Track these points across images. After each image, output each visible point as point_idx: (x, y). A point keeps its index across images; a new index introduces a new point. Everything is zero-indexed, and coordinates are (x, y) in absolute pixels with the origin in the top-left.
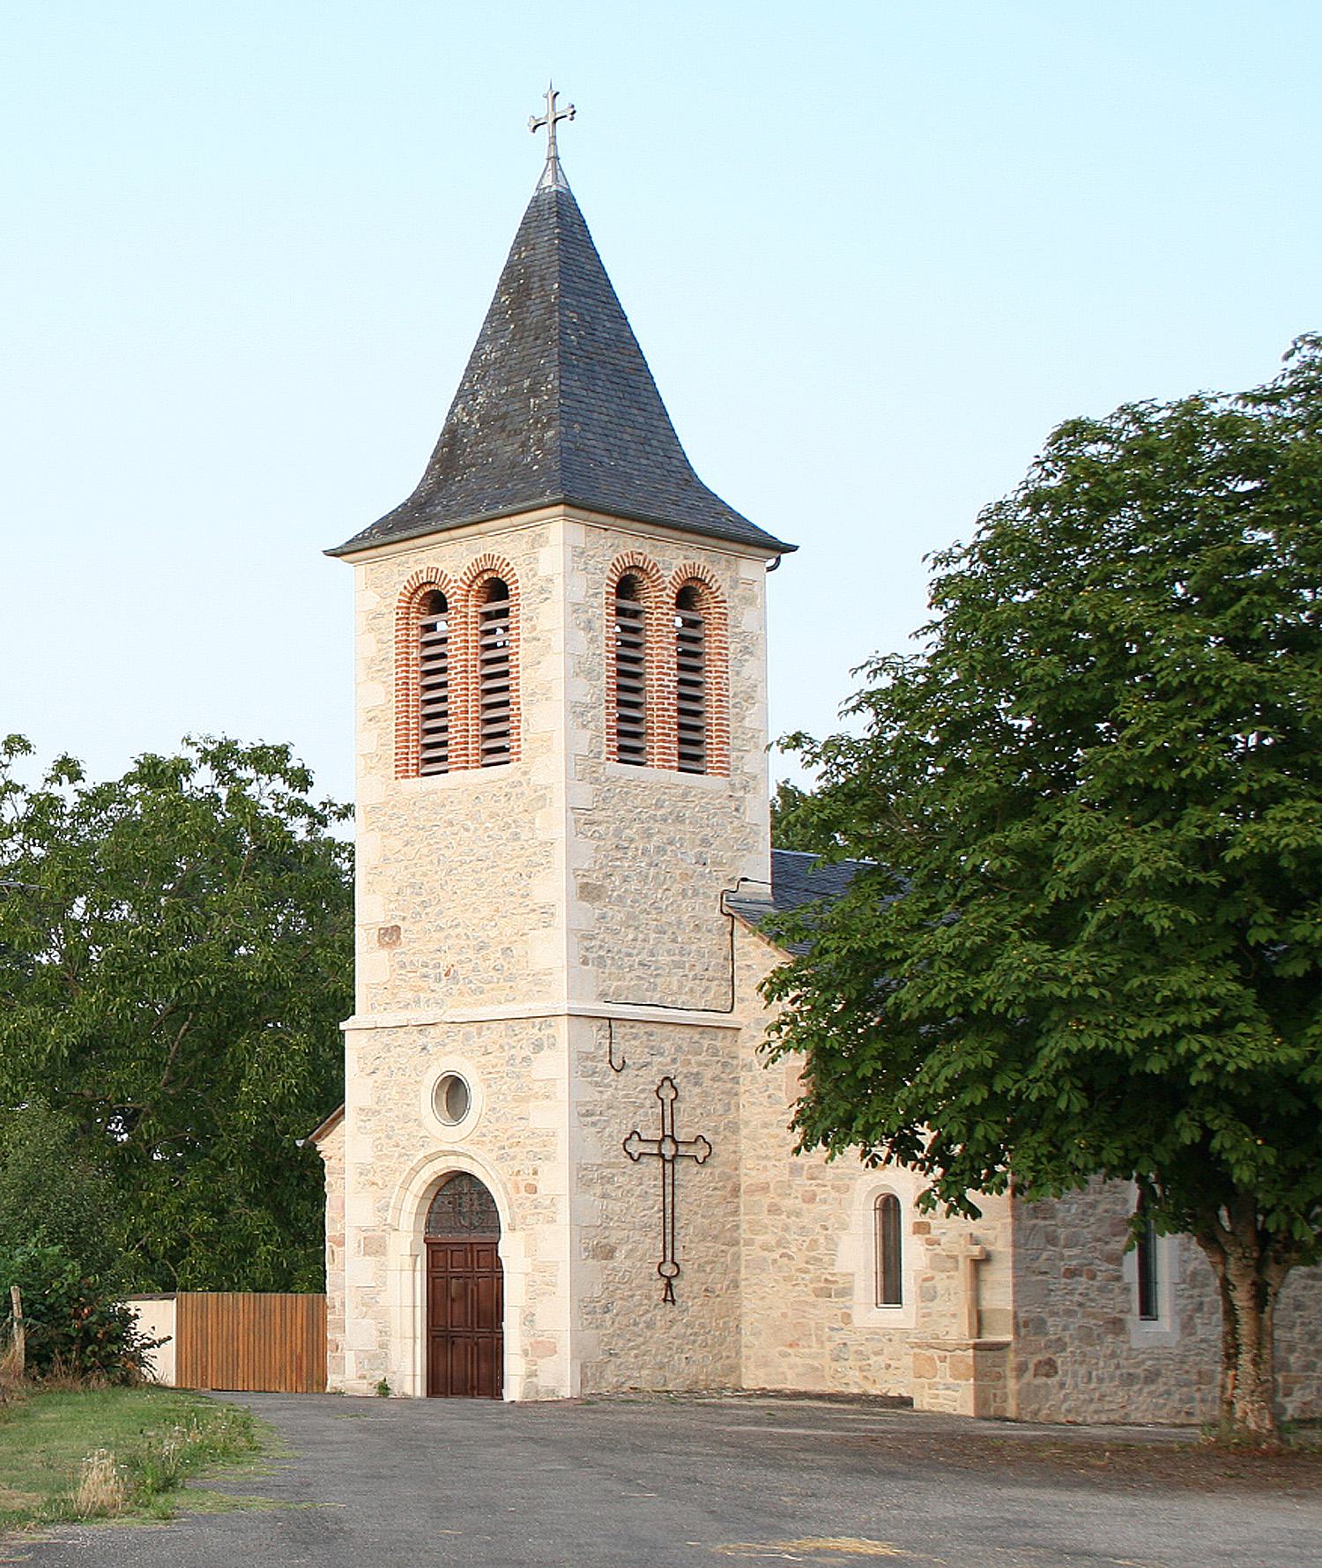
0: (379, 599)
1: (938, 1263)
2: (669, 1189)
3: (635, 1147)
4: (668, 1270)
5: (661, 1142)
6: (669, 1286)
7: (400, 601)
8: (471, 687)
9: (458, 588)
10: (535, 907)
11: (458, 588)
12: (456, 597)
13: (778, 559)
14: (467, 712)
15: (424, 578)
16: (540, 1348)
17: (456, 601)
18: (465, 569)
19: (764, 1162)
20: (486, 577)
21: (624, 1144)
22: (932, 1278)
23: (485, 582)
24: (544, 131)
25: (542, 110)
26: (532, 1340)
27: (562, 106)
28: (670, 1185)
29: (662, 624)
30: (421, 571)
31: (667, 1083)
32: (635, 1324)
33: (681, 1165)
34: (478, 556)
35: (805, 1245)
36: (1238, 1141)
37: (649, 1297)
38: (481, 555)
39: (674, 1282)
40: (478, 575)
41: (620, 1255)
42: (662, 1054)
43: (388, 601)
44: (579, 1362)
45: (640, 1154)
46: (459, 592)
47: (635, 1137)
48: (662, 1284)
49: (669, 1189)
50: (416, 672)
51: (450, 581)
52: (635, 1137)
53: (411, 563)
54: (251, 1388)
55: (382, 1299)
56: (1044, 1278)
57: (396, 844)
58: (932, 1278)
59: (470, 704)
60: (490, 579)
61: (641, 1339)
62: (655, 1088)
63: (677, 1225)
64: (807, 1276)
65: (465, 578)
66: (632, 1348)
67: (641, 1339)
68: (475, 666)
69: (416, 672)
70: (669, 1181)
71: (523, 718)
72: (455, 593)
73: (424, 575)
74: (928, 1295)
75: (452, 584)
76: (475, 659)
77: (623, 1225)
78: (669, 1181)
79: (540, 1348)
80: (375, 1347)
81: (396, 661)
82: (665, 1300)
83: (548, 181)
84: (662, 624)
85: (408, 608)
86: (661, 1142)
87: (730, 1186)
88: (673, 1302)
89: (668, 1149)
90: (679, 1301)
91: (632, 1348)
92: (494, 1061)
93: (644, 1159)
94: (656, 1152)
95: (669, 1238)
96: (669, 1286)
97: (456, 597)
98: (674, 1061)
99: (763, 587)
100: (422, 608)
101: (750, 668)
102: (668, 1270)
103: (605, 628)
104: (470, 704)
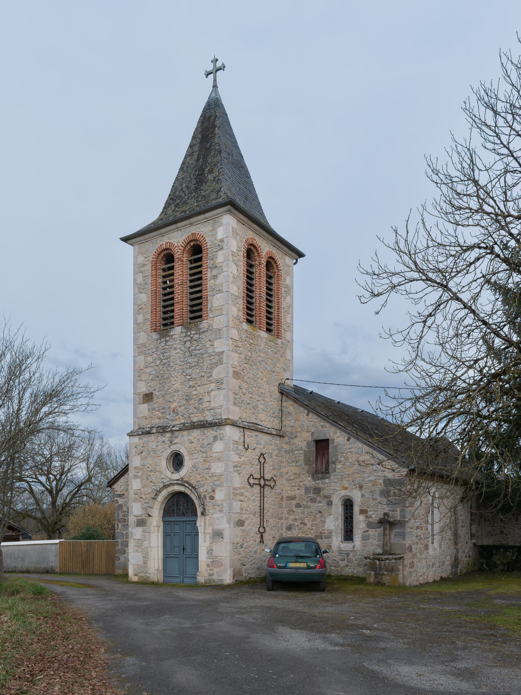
0: (143, 258)
1: (370, 525)
2: (262, 498)
3: (252, 481)
4: (262, 530)
5: (260, 479)
6: (262, 537)
7: (153, 258)
8: (185, 291)
9: (180, 249)
10: (214, 380)
11: (180, 249)
12: (179, 253)
13: (297, 260)
14: (183, 302)
15: (164, 247)
16: (215, 563)
17: (178, 255)
18: (183, 241)
19: (294, 488)
20: (192, 244)
21: (248, 480)
22: (368, 531)
23: (191, 246)
24: (211, 76)
25: (210, 67)
26: (212, 560)
27: (219, 64)
28: (262, 496)
29: (260, 272)
30: (163, 244)
31: (262, 456)
32: (251, 552)
33: (267, 489)
34: (189, 235)
35: (311, 519)
36: (457, 481)
37: (255, 541)
38: (190, 234)
39: (264, 534)
40: (189, 243)
41: (246, 524)
42: (260, 444)
43: (148, 259)
44: (232, 569)
45: (254, 484)
46: (180, 251)
47: (252, 477)
48: (259, 536)
49: (262, 498)
50: (160, 288)
51: (176, 247)
52: (252, 477)
53: (158, 241)
54: (83, 573)
55: (146, 543)
56: (411, 530)
57: (150, 359)
58: (368, 531)
59: (184, 298)
60: (194, 245)
61: (253, 558)
62: (258, 457)
63: (265, 512)
64: (312, 531)
65: (183, 245)
66: (250, 562)
67: (253, 558)
68: (187, 282)
69: (160, 288)
70: (262, 495)
71: (209, 301)
72: (178, 252)
73: (164, 246)
74: (365, 538)
75: (177, 248)
76: (187, 280)
77: (247, 512)
78: (262, 495)
79: (215, 563)
80: (141, 563)
81: (151, 283)
82: (260, 542)
83: (214, 95)
84: (260, 272)
85: (156, 261)
86: (260, 479)
87: (280, 497)
88: (263, 542)
89: (262, 482)
90: (265, 542)
91: (250, 562)
92: (195, 446)
93: (254, 486)
94: (258, 483)
95: (262, 517)
96: (262, 537)
97: (179, 253)
98: (264, 447)
99: (292, 270)
100: (162, 262)
101: (288, 299)
102: (262, 530)
103: (24, 569)
104: (184, 298)
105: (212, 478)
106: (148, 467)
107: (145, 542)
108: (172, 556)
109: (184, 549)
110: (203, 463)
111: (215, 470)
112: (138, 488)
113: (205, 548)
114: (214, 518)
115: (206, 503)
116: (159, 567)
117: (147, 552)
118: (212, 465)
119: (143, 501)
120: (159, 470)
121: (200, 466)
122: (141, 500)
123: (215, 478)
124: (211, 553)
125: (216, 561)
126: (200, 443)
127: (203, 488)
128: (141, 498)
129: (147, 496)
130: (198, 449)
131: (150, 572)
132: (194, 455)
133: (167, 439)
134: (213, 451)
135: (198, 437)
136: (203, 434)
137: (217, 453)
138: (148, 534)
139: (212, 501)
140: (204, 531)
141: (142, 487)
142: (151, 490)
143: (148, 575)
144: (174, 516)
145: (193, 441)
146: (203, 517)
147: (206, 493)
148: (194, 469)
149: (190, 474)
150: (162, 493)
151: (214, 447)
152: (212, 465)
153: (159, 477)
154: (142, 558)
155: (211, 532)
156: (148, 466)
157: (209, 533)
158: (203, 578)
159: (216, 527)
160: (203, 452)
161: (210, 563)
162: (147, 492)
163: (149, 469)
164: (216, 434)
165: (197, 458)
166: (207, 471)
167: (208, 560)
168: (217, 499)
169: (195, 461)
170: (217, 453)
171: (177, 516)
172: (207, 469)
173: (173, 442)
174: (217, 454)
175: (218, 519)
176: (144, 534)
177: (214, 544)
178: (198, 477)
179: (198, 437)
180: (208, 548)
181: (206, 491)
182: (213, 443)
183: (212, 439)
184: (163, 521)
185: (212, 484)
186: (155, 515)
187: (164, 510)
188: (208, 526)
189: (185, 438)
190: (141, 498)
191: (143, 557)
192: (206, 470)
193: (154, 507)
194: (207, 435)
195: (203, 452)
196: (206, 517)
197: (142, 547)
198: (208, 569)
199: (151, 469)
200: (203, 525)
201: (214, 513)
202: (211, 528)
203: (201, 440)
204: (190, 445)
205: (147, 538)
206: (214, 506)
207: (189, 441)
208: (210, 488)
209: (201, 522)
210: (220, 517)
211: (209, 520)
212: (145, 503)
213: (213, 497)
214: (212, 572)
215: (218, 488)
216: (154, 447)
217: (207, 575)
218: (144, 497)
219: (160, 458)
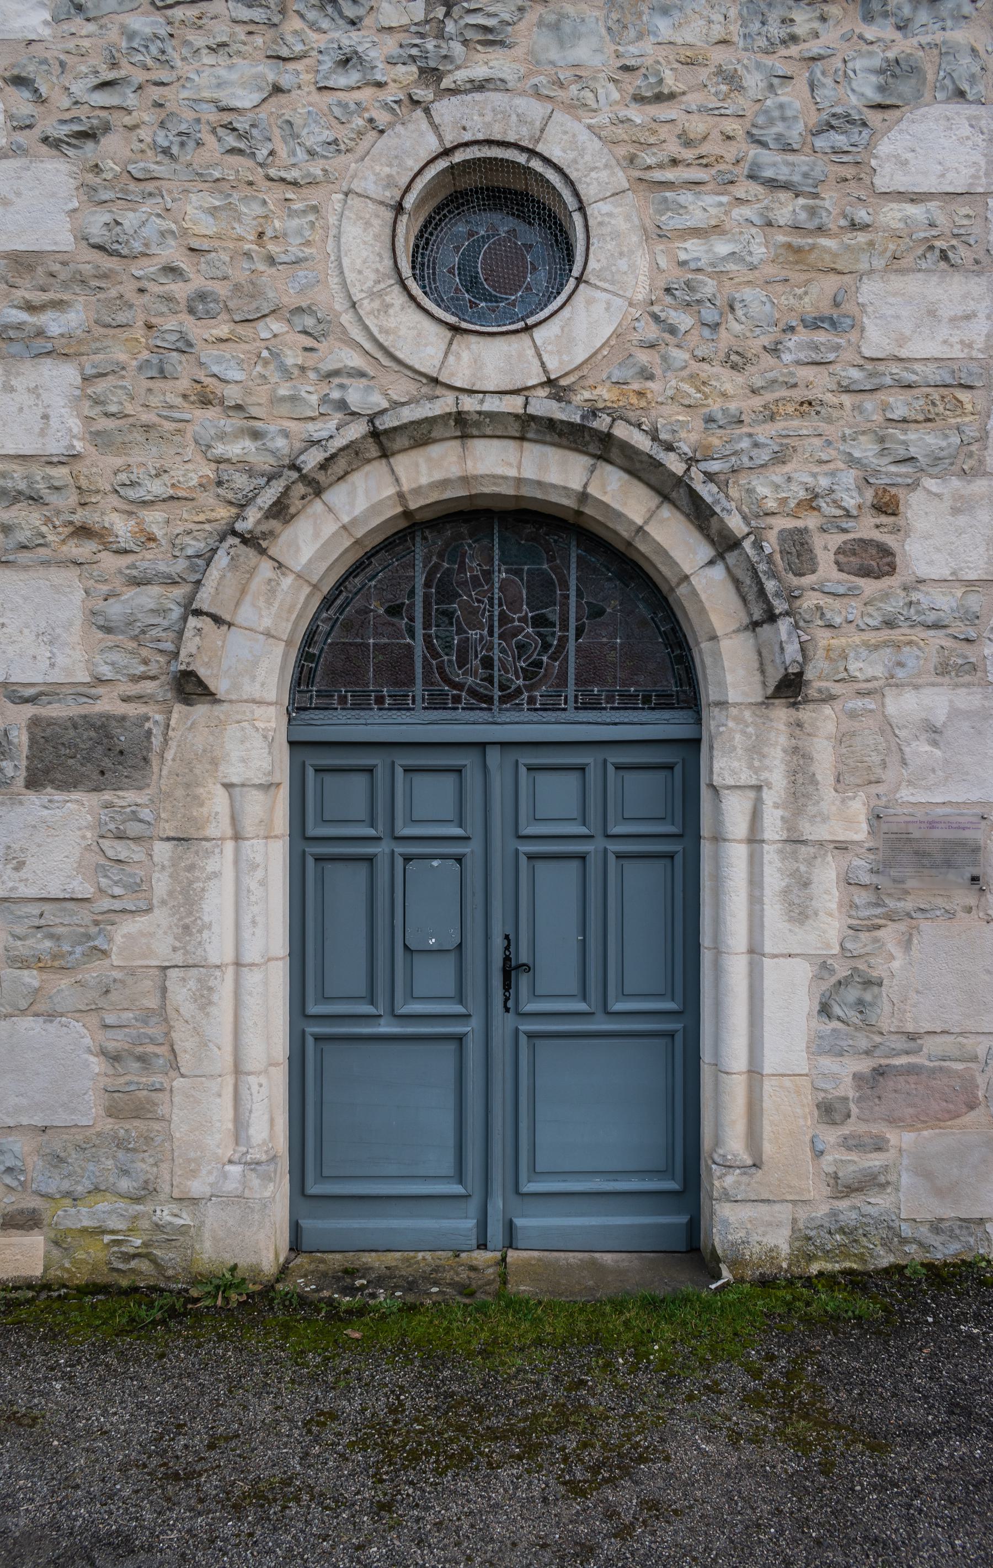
26: (864, 1066)
105: (869, 403)
106: (171, 270)
107: (129, 927)
108: (385, 1028)
109: (510, 971)
110: (770, 271)
111: (902, 340)
112: (54, 447)
113: (803, 971)
114: (888, 727)
115: (809, 601)
116: (272, 1137)
117: (162, 1013)
118: (869, 290)
119: (110, 562)
120: (291, 300)
121: (748, 294)
122: (83, 550)
123: (900, 405)
124: (861, 1005)
125: (912, 1070)
126: (740, 102)
127: (777, 475)
128: (83, 532)
129: (154, 519)
130: (729, 153)
131: (197, 1187)
132: (686, 198)
133: (390, 45)
134: (881, 183)
135: (719, 56)
136: (775, 30)
137: (915, 198)
138: (162, 851)
139: (869, 586)
140: (790, 825)
141: (99, 439)
142: (208, 471)
143: (165, 1215)
144: (400, 704)
145: (671, 82)
146: (781, 714)
147: (811, 521)
148: (684, 320)
149: (643, 357)
150: (336, 496)
151: (884, 147)
152: (869, 290)
153: (292, 358)
154: (97, 1064)
155: (860, 833)
156: (171, 253)
157: (842, 847)
158: (783, 1212)
159: (906, 794)
160: (773, 185)
161: (847, 1089)
162: (157, 488)
163: (180, 290)
164: (903, 46)
165: (717, 229)
166: (821, 337)
167: (828, 1063)
168: (923, 571)
169: (693, 249)
170: (915, 198)
171: (436, 702)
172: (814, 324)
173: (446, 83)
174: (913, 210)
175: (933, 731)
176: (121, 850)
177: (890, 934)
178: (729, 382)
179: (719, 56)
180: (824, 967)
181: (811, 503)
182: (874, 118)
183: (867, 87)
184: (292, 744)
185: (866, 449)
186: (251, 689)
187: (305, 656)
188: (828, 794)
189: (583, 52)
190: (83, 532)
191: (114, 1058)
192: (802, 335)
193: (246, 615)
194: (814, 48)
195: (773, 185)
196: (805, 714)
197: (93, 972)
198: (831, 1136)
199: (197, 282)
200: (777, 777)
201: (892, 681)
202: (858, 807)
203: (753, 81)
204: (637, 114)
205: (161, 885)
206: (889, 624)
207: (635, 83)
208: (849, 477)
209: (756, 750)
210: (955, 713)
211: (841, 739)
212: (137, 582)
213: (885, 551)
214: (874, 1161)
215: (930, 483)
216: (245, 99)
217: (815, 1190)
218: (122, 527)
219: (314, 196)
